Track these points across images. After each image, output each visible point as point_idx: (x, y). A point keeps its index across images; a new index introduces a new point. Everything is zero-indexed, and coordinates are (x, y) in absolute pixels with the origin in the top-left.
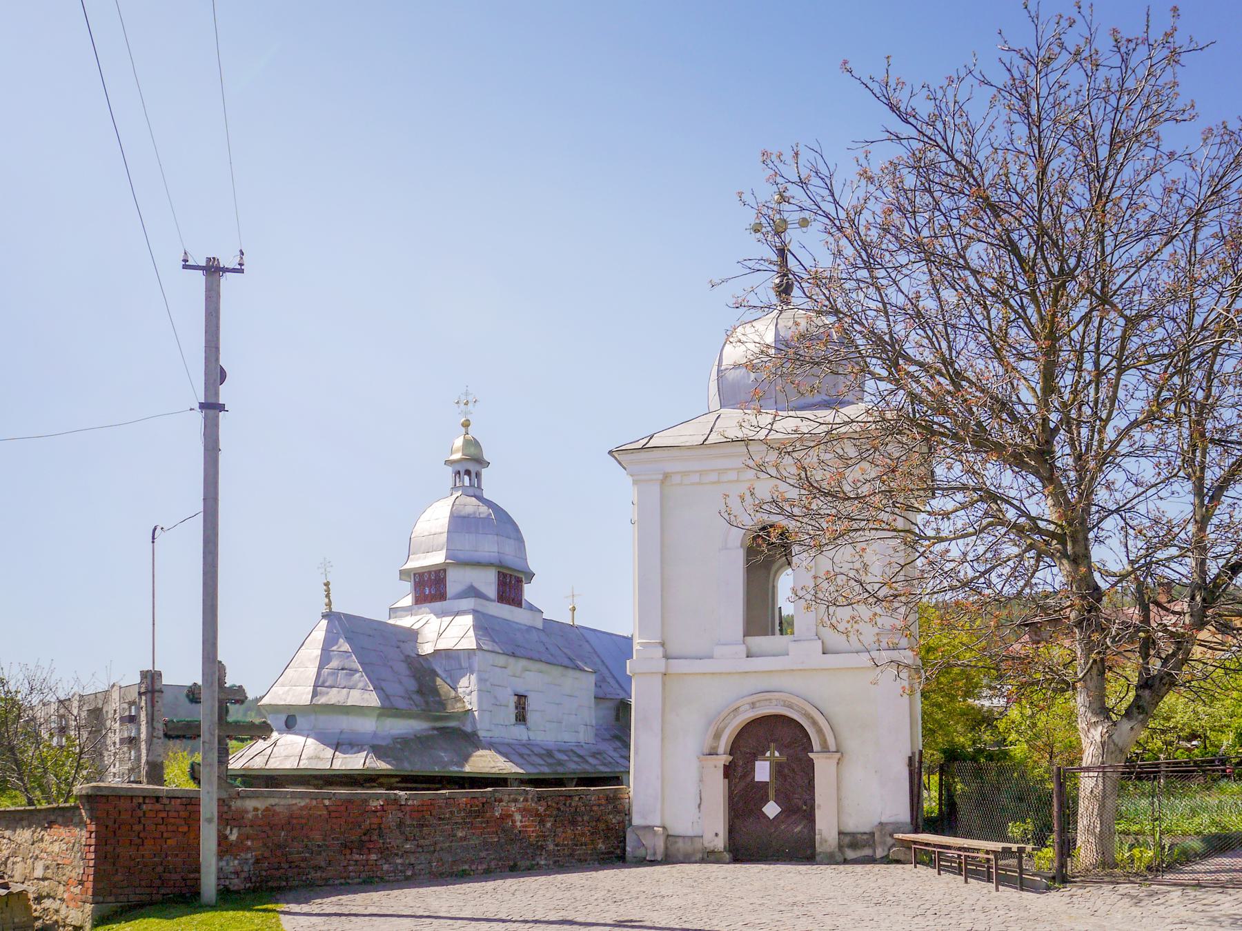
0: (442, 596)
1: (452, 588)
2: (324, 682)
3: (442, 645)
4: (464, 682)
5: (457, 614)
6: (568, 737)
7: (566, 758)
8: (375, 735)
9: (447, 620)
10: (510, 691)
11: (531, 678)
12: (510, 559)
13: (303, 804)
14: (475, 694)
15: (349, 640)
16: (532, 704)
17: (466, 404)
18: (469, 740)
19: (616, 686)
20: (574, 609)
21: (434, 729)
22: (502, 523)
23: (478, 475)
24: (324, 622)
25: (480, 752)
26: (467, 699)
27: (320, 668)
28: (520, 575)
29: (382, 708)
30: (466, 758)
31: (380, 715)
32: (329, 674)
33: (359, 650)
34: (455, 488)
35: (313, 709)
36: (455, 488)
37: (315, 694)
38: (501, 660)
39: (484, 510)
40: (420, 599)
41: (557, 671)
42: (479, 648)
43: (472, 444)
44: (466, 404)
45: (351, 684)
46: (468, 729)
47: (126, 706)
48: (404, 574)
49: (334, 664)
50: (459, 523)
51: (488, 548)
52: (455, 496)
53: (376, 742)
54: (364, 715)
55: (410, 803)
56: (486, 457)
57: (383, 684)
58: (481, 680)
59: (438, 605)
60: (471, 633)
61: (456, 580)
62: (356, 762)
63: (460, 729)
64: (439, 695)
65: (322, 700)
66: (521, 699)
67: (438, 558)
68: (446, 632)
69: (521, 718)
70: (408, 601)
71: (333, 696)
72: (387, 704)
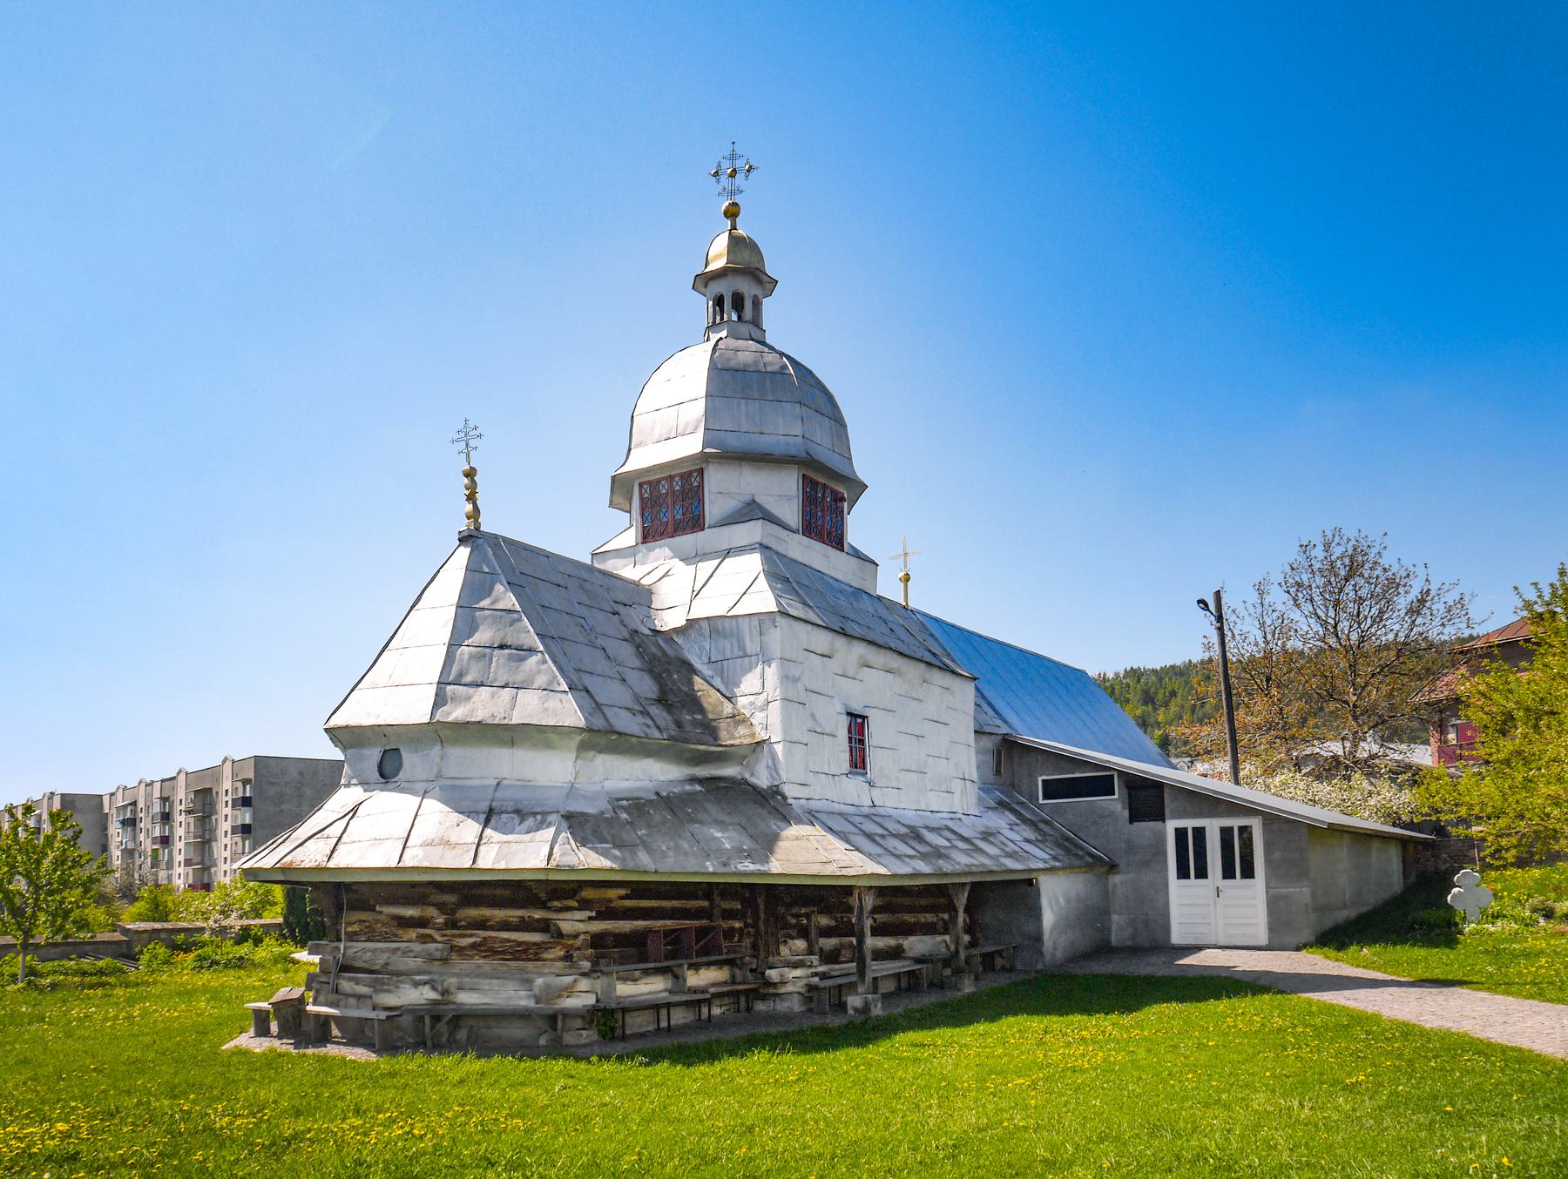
0: (696, 523)
1: (714, 508)
2: (461, 675)
3: (701, 610)
4: (749, 683)
5: (728, 553)
7: (946, 843)
8: (572, 791)
9: (707, 567)
10: (839, 708)
11: (877, 684)
14: (775, 708)
16: (877, 733)
17: (733, 174)
20: (907, 578)
23: (757, 304)
24: (464, 552)
25: (794, 830)
27: (453, 645)
28: (841, 489)
30: (768, 844)
31: (583, 747)
32: (471, 657)
33: (535, 609)
35: (437, 733)
37: (440, 700)
38: (822, 640)
41: (914, 671)
43: (736, 243)
44: (733, 174)
46: (762, 780)
47: (240, 785)
48: (621, 486)
49: (484, 636)
50: (727, 380)
51: (785, 428)
52: (714, 337)
54: (549, 745)
56: (771, 269)
57: (588, 681)
58: (787, 679)
60: (762, 582)
61: (724, 489)
62: (527, 852)
63: (745, 782)
64: (702, 710)
65: (456, 713)
67: (693, 445)
68: (707, 587)
69: (857, 723)
70: (630, 538)
71: (481, 706)
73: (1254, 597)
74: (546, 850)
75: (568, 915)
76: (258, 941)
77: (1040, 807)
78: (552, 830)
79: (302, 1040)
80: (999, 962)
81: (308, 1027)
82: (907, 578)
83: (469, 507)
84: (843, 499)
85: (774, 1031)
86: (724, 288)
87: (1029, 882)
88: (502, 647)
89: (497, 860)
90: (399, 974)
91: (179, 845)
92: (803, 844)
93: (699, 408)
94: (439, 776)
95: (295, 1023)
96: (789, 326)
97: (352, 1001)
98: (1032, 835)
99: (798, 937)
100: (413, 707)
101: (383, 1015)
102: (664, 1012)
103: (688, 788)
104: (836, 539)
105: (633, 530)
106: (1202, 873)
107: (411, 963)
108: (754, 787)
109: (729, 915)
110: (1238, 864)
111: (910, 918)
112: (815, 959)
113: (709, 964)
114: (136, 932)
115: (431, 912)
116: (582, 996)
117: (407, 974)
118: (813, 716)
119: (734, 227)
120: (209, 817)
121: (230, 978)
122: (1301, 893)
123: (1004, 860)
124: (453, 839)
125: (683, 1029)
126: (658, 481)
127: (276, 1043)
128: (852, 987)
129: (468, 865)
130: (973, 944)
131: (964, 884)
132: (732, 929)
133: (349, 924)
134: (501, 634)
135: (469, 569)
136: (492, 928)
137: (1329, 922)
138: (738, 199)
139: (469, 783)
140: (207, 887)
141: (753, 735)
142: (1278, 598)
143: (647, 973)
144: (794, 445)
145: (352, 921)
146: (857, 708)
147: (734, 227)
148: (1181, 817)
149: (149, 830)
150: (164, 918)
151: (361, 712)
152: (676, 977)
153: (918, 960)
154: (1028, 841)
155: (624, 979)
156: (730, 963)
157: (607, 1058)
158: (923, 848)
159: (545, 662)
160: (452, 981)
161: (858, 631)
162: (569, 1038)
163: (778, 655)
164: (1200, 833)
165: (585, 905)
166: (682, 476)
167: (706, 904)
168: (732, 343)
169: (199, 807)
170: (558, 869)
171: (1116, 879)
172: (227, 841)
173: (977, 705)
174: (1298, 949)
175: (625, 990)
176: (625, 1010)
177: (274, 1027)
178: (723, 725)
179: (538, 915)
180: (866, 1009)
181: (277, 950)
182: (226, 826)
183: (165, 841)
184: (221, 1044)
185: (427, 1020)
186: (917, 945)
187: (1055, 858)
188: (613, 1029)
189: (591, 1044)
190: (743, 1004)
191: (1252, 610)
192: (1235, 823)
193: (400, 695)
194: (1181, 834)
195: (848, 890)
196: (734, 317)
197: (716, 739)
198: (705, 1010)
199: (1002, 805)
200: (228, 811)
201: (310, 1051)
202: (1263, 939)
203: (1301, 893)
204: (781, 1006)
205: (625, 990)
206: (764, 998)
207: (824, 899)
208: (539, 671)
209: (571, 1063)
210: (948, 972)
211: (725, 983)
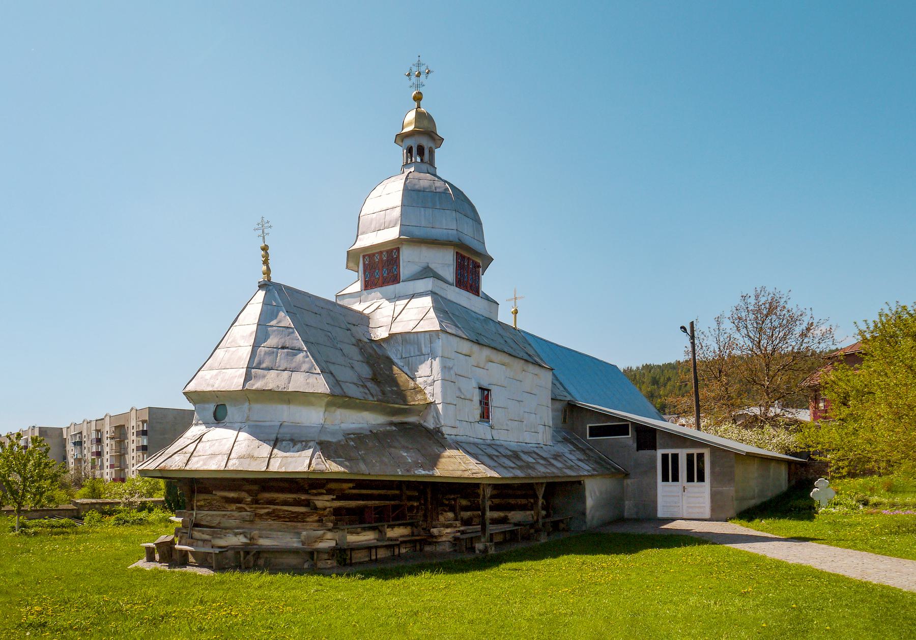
0: (395, 279)
1: (405, 270)
2: (260, 363)
3: (397, 329)
5: (413, 296)
10: (475, 385)
11: (496, 371)
14: (438, 384)
16: (496, 400)
17: (418, 75)
19: (562, 389)
20: (516, 312)
21: (391, 424)
22: (459, 203)
23: (432, 153)
24: (261, 294)
25: (448, 452)
26: (428, 390)
27: (255, 346)
29: (332, 395)
30: (434, 461)
31: (329, 405)
32: (266, 353)
33: (302, 326)
34: (406, 165)
35: (245, 396)
36: (406, 165)
37: (248, 377)
38: (466, 347)
39: (438, 184)
40: (369, 285)
41: (518, 365)
42: (443, 331)
43: (420, 116)
44: (418, 75)
45: (293, 365)
46: (430, 424)
48: (353, 256)
49: (273, 341)
51: (446, 224)
52: (407, 171)
53: (324, 438)
56: (440, 132)
57: (332, 368)
58: (445, 368)
59: (390, 288)
60: (432, 314)
61: (410, 260)
62: (298, 462)
63: (420, 425)
65: (257, 385)
66: (485, 392)
67: (393, 234)
69: (485, 415)
70: (357, 287)
71: (271, 381)
72: (338, 391)
73: (715, 325)
74: (308, 462)
75: (320, 498)
76: (150, 510)
77: (588, 441)
78: (311, 450)
79: (173, 563)
80: (562, 526)
81: (176, 556)
82: (516, 312)
83: (265, 268)
84: (479, 266)
86: (413, 142)
88: (283, 348)
89: (204, 464)
90: (226, 528)
91: (107, 457)
92: (452, 460)
93: (398, 212)
94: (248, 419)
95: (168, 554)
96: (449, 165)
97: (200, 543)
98: (582, 457)
99: (450, 511)
102: (373, 551)
103: (388, 428)
104: (474, 288)
105: (359, 283)
106: (676, 479)
107: (233, 523)
109: (410, 498)
110: (696, 474)
111: (512, 501)
112: (458, 523)
113: (399, 525)
115: (244, 495)
116: (328, 542)
118: (459, 389)
120: (123, 441)
121: (135, 530)
123: (565, 470)
124: (256, 455)
126: (374, 255)
127: (158, 565)
128: (478, 539)
131: (542, 483)
133: (198, 501)
134: (283, 341)
136: (278, 504)
138: (421, 90)
141: (426, 399)
142: (728, 325)
143: (364, 529)
144: (452, 235)
145: (200, 499)
146: (485, 385)
148: (664, 447)
149: (90, 448)
152: (380, 532)
153: (515, 525)
154: (579, 460)
155: (352, 533)
157: (341, 575)
159: (307, 356)
161: (485, 341)
162: (320, 564)
163: (440, 354)
164: (675, 457)
165: (330, 492)
166: (387, 252)
167: (397, 492)
168: (417, 175)
170: (314, 472)
171: (628, 482)
174: (726, 521)
175: (352, 538)
176: (352, 549)
177: (157, 557)
179: (303, 497)
180: (485, 550)
181: (162, 515)
182: (133, 446)
183: (99, 454)
185: (242, 553)
186: (516, 516)
187: (594, 470)
188: (345, 560)
190: (418, 547)
191: (713, 333)
192: (695, 451)
193: (226, 374)
194: (665, 457)
195: (477, 486)
196: (419, 160)
198: (397, 551)
199: (566, 440)
200: (134, 438)
201: (177, 570)
202: (707, 515)
203: (729, 490)
204: (439, 548)
205: (352, 538)
206: (430, 544)
208: (304, 362)
210: (532, 531)
211: (408, 536)
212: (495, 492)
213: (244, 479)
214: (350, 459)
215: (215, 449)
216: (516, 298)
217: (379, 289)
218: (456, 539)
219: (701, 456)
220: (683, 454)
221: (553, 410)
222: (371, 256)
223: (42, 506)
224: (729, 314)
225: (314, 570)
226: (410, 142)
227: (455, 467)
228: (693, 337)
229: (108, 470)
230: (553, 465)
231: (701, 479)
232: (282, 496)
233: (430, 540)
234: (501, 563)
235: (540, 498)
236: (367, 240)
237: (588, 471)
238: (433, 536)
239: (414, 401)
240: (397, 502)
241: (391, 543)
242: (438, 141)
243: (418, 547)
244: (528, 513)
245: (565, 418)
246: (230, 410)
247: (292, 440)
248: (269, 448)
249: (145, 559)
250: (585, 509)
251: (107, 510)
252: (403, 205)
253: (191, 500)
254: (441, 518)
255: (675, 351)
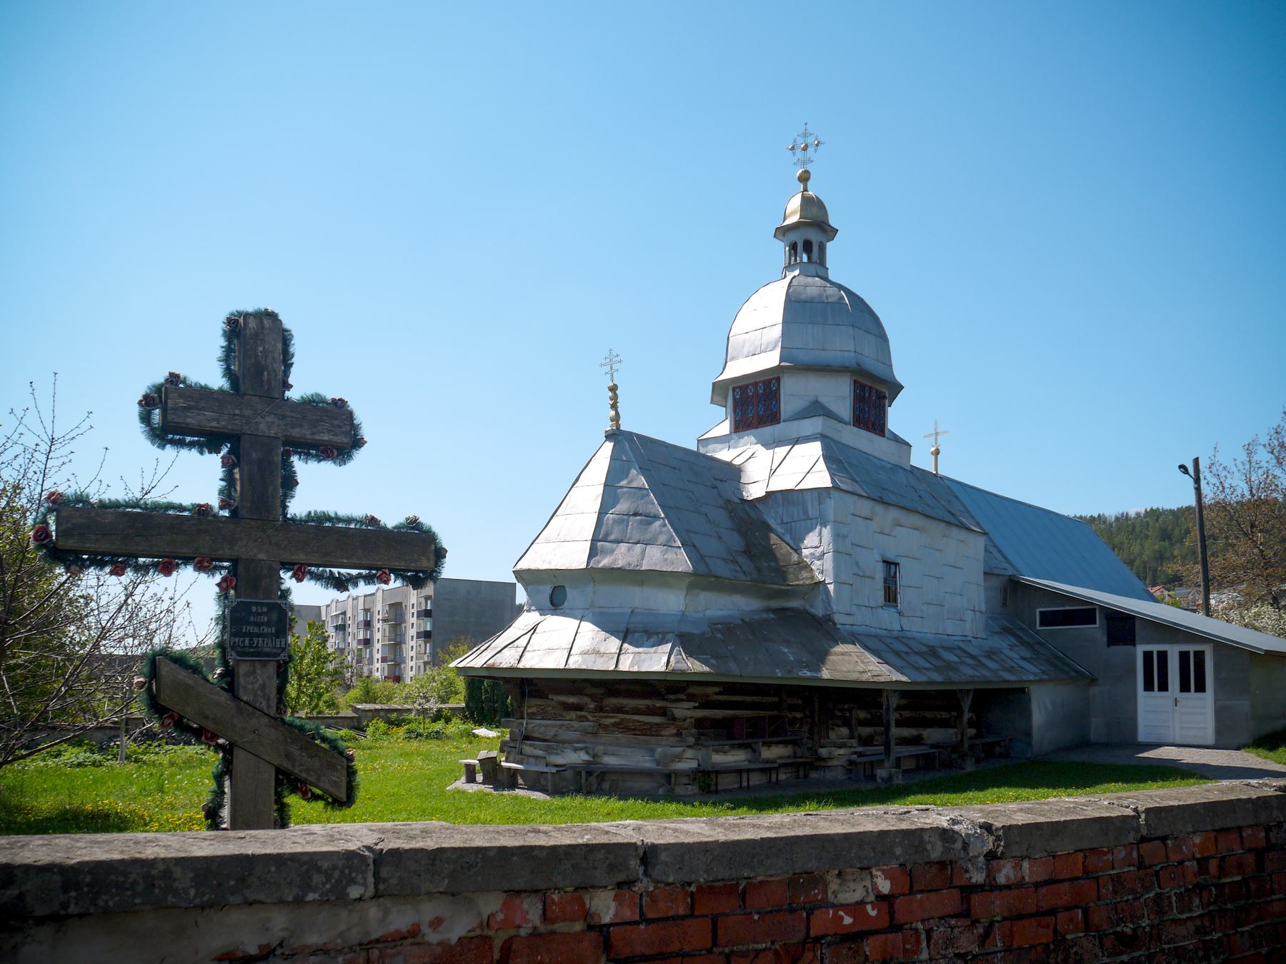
0: (772, 417)
2: (607, 534)
3: (776, 485)
4: (811, 540)
5: (797, 441)
6: (951, 628)
9: (781, 451)
10: (878, 557)
11: (906, 538)
12: (871, 364)
13: (459, 928)
14: (829, 557)
15: (644, 470)
16: (906, 576)
17: (805, 149)
18: (822, 631)
19: (1001, 558)
20: (937, 453)
21: (769, 610)
22: (859, 315)
23: (822, 249)
26: (816, 565)
27: (602, 513)
29: (695, 574)
30: (820, 657)
32: (615, 521)
34: (789, 267)
35: (589, 575)
36: (789, 267)
37: (593, 552)
38: (865, 507)
39: (832, 291)
40: (742, 425)
41: (936, 528)
42: (835, 487)
43: (810, 204)
44: (805, 149)
45: (648, 536)
46: (819, 611)
47: (423, 600)
48: (721, 390)
49: (622, 507)
50: (796, 307)
51: (841, 345)
52: (790, 276)
55: (1005, 874)
58: (838, 537)
59: (767, 430)
60: (822, 465)
61: (793, 393)
62: (655, 660)
64: (776, 559)
65: (605, 562)
67: (771, 360)
68: (783, 467)
69: (891, 596)
70: (725, 428)
71: (621, 556)
73: (1243, 456)
74: (665, 659)
75: (679, 705)
76: (448, 720)
77: (1038, 632)
78: (670, 645)
79: (498, 786)
80: (998, 750)
81: (503, 777)
82: (937, 453)
83: (613, 413)
84: (884, 397)
85: (822, 791)
86: (798, 237)
87: (1022, 690)
88: (635, 514)
89: (632, 665)
90: (563, 742)
91: (378, 646)
92: (846, 658)
93: (777, 331)
94: (592, 606)
95: (494, 775)
96: (845, 264)
97: (532, 760)
98: (1027, 654)
99: (844, 725)
100: (574, 556)
101: (554, 770)
102: (745, 776)
103: (764, 616)
105: (727, 422)
106: (1164, 687)
107: (572, 735)
108: (813, 616)
109: (793, 708)
110: (1193, 679)
111: (929, 715)
112: (854, 742)
113: (778, 743)
114: (364, 711)
115: (586, 700)
116: (688, 763)
117: (569, 742)
118: (857, 564)
119: (805, 190)
120: (400, 625)
121: (433, 746)
122: (1243, 704)
123: (1002, 673)
124: (602, 650)
125: (758, 788)
126: (747, 386)
127: (483, 787)
128: (881, 762)
129: (612, 668)
130: (978, 736)
131: (969, 691)
132: (795, 719)
133: (529, 707)
135: (613, 458)
136: (627, 713)
137: (1268, 728)
138: (809, 167)
139: (611, 611)
140: (398, 679)
141: (813, 578)
142: (1263, 456)
143: (733, 747)
145: (532, 705)
146: (891, 556)
147: (805, 190)
148: (1148, 643)
149: (356, 633)
150: (374, 700)
151: (539, 559)
152: (754, 751)
153: (933, 746)
154: (1024, 659)
155: (717, 752)
156: (794, 743)
157: (706, 804)
158: (938, 663)
159: (665, 525)
160: (600, 749)
161: (893, 499)
162: (679, 790)
163: (831, 518)
164: (1163, 656)
165: (691, 698)
166: (764, 382)
167: (776, 699)
168: (803, 280)
169: (392, 616)
170: (673, 672)
171: (1095, 690)
172: (413, 643)
173: (986, 550)
174: (1238, 749)
175: (718, 759)
176: (718, 772)
177: (479, 777)
178: (791, 570)
179: (658, 704)
180: (890, 778)
181: (462, 727)
182: (412, 632)
183: (367, 642)
184: (446, 785)
185: (584, 774)
186: (933, 735)
187: (1044, 672)
188: (709, 785)
189: (694, 795)
190: (802, 773)
191: (1241, 467)
192: (1192, 648)
193: (566, 548)
194: (1148, 656)
197: (785, 580)
198: (774, 776)
199: (1006, 631)
200: (414, 620)
201: (505, 793)
202: (1210, 739)
203: (1243, 704)
204: (829, 775)
205: (718, 759)
206: (817, 768)
207: (863, 697)
208: (661, 532)
209: (681, 806)
210: (955, 756)
211: (789, 757)
212: (903, 702)
213: (586, 680)
214: (717, 657)
215: (551, 643)
216: (937, 434)
217: (753, 431)
218: (851, 763)
219: (1200, 656)
220: (1173, 652)
221: (986, 589)
222: (743, 389)
223: (320, 712)
224: (1265, 440)
225: (671, 797)
226: (793, 237)
227: (850, 667)
228: (1197, 480)
229: (378, 665)
230: (984, 665)
231: (1201, 688)
232: (631, 703)
233: (817, 764)
234: (908, 795)
235: (966, 710)
236: (739, 368)
237: (1035, 674)
238: (821, 759)
239: (798, 580)
240: (775, 713)
241: (768, 766)
242: (829, 232)
243: (802, 773)
244: (952, 731)
245: (1005, 599)
246: (570, 593)
247: (645, 631)
248: (617, 642)
249: (463, 779)
250: (1030, 728)
251: (394, 719)
252: (784, 322)
253: (521, 705)
254: (832, 735)
255: (1179, 496)
